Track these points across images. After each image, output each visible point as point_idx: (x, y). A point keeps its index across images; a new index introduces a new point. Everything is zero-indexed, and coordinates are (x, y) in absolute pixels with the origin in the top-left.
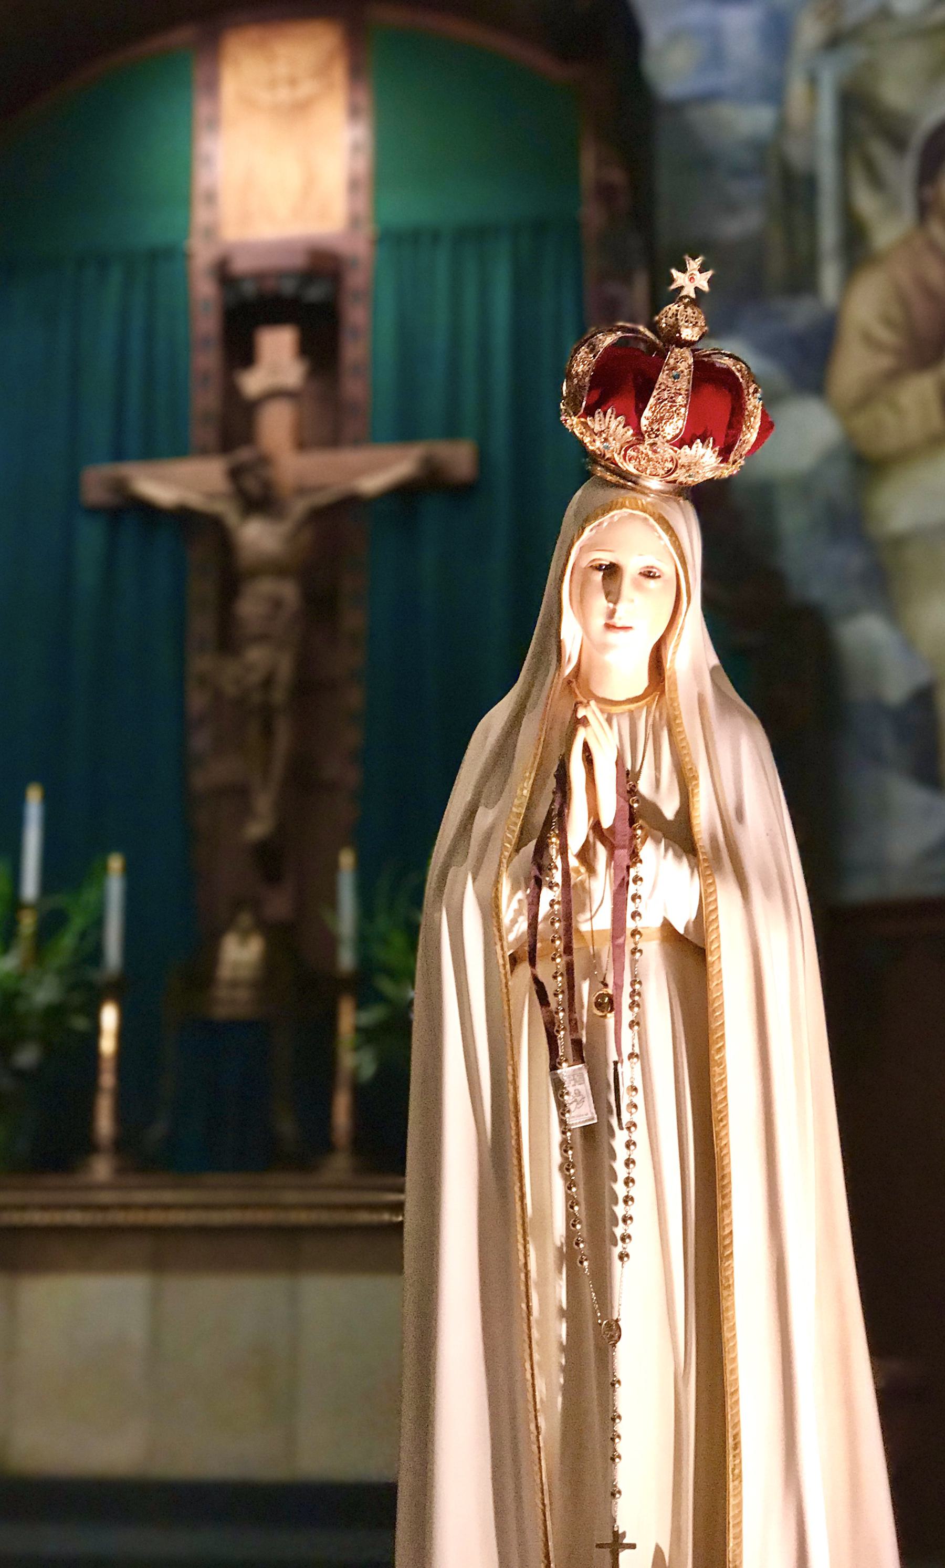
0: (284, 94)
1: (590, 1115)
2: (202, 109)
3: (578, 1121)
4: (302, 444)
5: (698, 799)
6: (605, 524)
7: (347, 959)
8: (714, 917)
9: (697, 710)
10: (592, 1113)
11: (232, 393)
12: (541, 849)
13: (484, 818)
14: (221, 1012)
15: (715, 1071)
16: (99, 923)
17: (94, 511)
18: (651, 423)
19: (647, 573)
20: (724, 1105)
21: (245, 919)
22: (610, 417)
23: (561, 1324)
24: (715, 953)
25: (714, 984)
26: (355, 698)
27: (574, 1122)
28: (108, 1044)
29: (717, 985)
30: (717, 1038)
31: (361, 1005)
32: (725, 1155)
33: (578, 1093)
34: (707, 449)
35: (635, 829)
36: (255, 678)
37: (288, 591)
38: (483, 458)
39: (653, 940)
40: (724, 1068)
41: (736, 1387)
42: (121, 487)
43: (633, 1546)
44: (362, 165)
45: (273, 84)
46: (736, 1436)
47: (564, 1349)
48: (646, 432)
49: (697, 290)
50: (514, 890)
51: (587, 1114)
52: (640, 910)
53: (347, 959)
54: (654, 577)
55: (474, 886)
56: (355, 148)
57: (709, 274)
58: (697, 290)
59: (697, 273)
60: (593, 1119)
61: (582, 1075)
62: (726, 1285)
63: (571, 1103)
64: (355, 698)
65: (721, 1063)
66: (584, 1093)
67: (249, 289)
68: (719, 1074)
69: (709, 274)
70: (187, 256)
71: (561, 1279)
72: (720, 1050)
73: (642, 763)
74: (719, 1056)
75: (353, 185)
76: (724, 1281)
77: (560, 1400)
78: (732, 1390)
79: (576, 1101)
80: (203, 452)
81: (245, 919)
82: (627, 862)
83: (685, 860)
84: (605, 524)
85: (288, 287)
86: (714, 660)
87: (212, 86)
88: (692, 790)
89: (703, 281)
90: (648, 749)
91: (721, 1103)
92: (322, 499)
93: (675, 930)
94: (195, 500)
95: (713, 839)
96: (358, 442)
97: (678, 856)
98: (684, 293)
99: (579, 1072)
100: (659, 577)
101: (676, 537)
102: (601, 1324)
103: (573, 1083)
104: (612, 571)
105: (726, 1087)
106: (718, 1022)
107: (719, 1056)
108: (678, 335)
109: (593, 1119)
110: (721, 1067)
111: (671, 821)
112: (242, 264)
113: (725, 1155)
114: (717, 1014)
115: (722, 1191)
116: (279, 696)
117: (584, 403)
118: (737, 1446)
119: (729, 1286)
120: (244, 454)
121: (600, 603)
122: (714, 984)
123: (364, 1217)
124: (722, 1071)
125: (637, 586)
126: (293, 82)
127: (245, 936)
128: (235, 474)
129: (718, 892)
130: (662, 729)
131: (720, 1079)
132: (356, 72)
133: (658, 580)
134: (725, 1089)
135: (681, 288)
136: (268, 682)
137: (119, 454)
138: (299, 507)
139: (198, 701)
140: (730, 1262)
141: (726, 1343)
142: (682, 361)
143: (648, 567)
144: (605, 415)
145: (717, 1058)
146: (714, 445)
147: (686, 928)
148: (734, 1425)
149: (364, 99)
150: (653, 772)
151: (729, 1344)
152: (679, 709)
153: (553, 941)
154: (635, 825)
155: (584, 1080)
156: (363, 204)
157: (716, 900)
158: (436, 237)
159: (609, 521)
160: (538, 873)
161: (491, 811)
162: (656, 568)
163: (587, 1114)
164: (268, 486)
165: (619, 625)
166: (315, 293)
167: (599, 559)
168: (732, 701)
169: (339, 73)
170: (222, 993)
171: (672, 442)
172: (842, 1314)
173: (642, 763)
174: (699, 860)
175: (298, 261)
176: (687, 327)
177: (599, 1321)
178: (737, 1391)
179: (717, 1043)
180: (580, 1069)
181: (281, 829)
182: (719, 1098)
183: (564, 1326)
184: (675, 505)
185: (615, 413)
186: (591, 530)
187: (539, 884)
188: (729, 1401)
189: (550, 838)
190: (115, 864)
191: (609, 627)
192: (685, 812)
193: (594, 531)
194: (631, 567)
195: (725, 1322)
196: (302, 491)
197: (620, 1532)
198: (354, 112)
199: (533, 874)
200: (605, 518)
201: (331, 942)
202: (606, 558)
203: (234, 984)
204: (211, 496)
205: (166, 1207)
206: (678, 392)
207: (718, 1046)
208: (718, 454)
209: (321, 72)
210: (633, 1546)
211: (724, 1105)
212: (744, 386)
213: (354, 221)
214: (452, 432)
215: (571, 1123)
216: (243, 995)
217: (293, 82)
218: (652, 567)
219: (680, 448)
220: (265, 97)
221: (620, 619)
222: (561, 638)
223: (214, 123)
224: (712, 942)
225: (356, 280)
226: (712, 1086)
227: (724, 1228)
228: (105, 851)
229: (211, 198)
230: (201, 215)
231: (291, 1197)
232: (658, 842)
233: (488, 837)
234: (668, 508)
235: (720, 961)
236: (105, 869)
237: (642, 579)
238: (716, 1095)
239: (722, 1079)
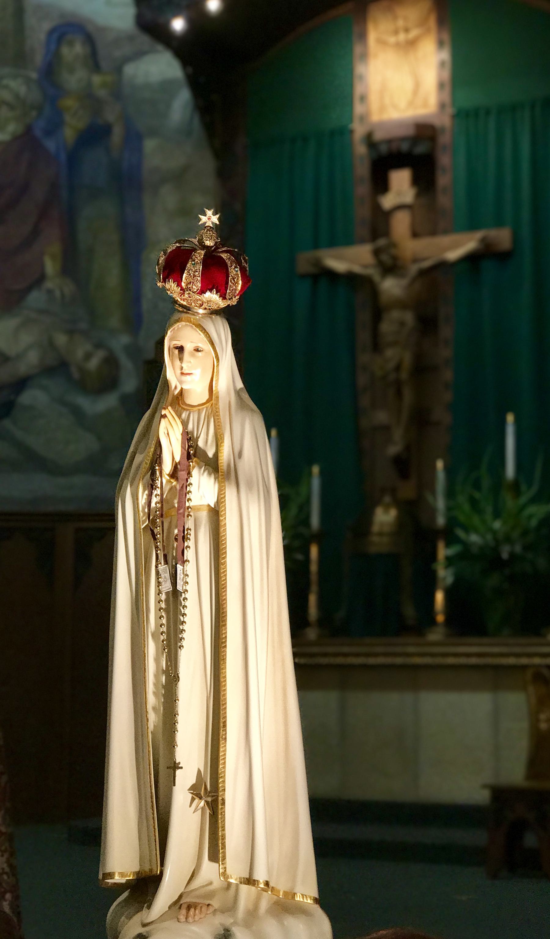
0: (402, 37)
1: (169, 587)
2: (358, 49)
3: (165, 589)
4: (415, 235)
5: (223, 448)
6: (176, 329)
7: (441, 521)
8: (223, 500)
9: (228, 409)
10: (170, 586)
11: (377, 208)
12: (153, 473)
13: (138, 458)
14: (373, 550)
15: (221, 567)
16: (308, 501)
17: (304, 276)
18: (187, 285)
19: (197, 349)
20: (224, 582)
21: (387, 499)
22: (171, 283)
23: (163, 676)
24: (223, 516)
25: (222, 529)
26: (448, 375)
27: (164, 590)
28: (314, 568)
29: (224, 530)
30: (223, 553)
31: (448, 545)
32: (224, 603)
33: (165, 578)
34: (213, 294)
35: (189, 463)
36: (391, 365)
37: (409, 317)
38: (516, 237)
39: (205, 511)
40: (226, 566)
41: (225, 702)
42: (318, 263)
43: (181, 768)
44: (446, 74)
45: (396, 32)
46: (225, 722)
47: (164, 687)
48: (185, 288)
49: (213, 223)
50: (144, 491)
51: (168, 586)
52: (191, 498)
53: (441, 521)
54: (200, 351)
55: (130, 488)
56: (442, 64)
57: (218, 216)
58: (213, 223)
59: (212, 216)
60: (170, 589)
61: (167, 569)
62: (222, 659)
63: (163, 582)
64: (448, 375)
65: (225, 563)
66: (167, 577)
67: (384, 149)
68: (223, 568)
69: (218, 216)
70: (351, 132)
71: (164, 658)
72: (224, 558)
73: (201, 432)
74: (223, 561)
75: (441, 86)
76: (221, 657)
77: (162, 708)
78: (223, 703)
79: (164, 581)
80: (362, 241)
81: (387, 499)
82: (186, 477)
83: (213, 476)
84: (176, 329)
85: (405, 147)
86: (240, 385)
87: (363, 36)
88: (220, 444)
89: (215, 219)
90: (204, 426)
91: (223, 581)
92: (426, 264)
93: (212, 507)
94: (357, 269)
95: (229, 466)
96: (446, 232)
97: (210, 474)
98: (207, 225)
99: (165, 568)
100: (202, 351)
101: (207, 333)
102: (171, 675)
103: (163, 573)
104: (181, 349)
105: (226, 574)
106: (223, 546)
107: (223, 561)
108: (203, 244)
109: (170, 589)
110: (224, 565)
111: (211, 458)
112: (378, 136)
113: (224, 603)
114: (223, 542)
115: (222, 619)
116: (404, 375)
117: (161, 276)
118: (225, 726)
119: (224, 659)
120: (382, 242)
121: (178, 363)
122: (222, 529)
123: (451, 661)
124: (224, 567)
125: (192, 355)
126: (407, 30)
127: (387, 508)
128: (377, 253)
129: (227, 489)
130: (211, 418)
131: (223, 570)
132: (441, 22)
133: (201, 352)
134: (226, 575)
135: (205, 223)
136: (398, 368)
137: (316, 246)
138: (414, 269)
139: (362, 380)
140: (225, 649)
141: (221, 683)
142: (199, 255)
143: (196, 347)
144: (169, 281)
145: (222, 561)
146: (217, 293)
147: (215, 505)
148: (223, 717)
149: (446, 37)
150: (206, 437)
151: (222, 684)
152: (219, 409)
153: (156, 512)
154: (189, 461)
155: (167, 572)
156: (447, 96)
157: (225, 493)
158: (488, 112)
159: (177, 327)
160: (152, 483)
161: (141, 455)
162: (201, 348)
163: (168, 586)
164: (395, 258)
165: (185, 373)
166: (421, 149)
167: (176, 344)
168: (248, 405)
169: (432, 22)
170: (375, 539)
171: (197, 292)
172: (284, 673)
173: (201, 432)
174: (219, 475)
175: (411, 132)
176: (207, 240)
177: (171, 674)
178: (226, 704)
179: (223, 555)
180: (166, 567)
181: (408, 448)
182: (223, 579)
183: (164, 677)
184: (209, 319)
185: (172, 281)
186: (171, 332)
187: (152, 488)
188: (221, 707)
189: (155, 467)
190: (316, 470)
191: (182, 374)
192: (216, 455)
193: (172, 332)
194: (189, 347)
195: (221, 674)
196: (415, 260)
197: (177, 762)
198: (441, 44)
199: (150, 483)
200: (175, 326)
201: (433, 511)
202: (179, 344)
203: (380, 534)
204: (365, 266)
205: (345, 655)
206: (196, 271)
207: (223, 556)
208: (220, 296)
209: (422, 23)
210: (181, 768)
211: (224, 582)
212: (229, 265)
213: (442, 106)
214: (499, 223)
215: (162, 590)
216: (385, 540)
217: (407, 30)
218: (198, 347)
219: (201, 295)
220: (392, 40)
221: (185, 370)
222: (168, 379)
223: (364, 56)
224: (222, 510)
225: (444, 139)
226: (220, 574)
227: (222, 634)
228: (310, 464)
229: (363, 99)
230: (358, 109)
231: (411, 649)
232: (200, 468)
233: (139, 467)
234: (204, 321)
235: (225, 519)
236: (310, 474)
237: (194, 352)
238: (221, 577)
239: (224, 571)
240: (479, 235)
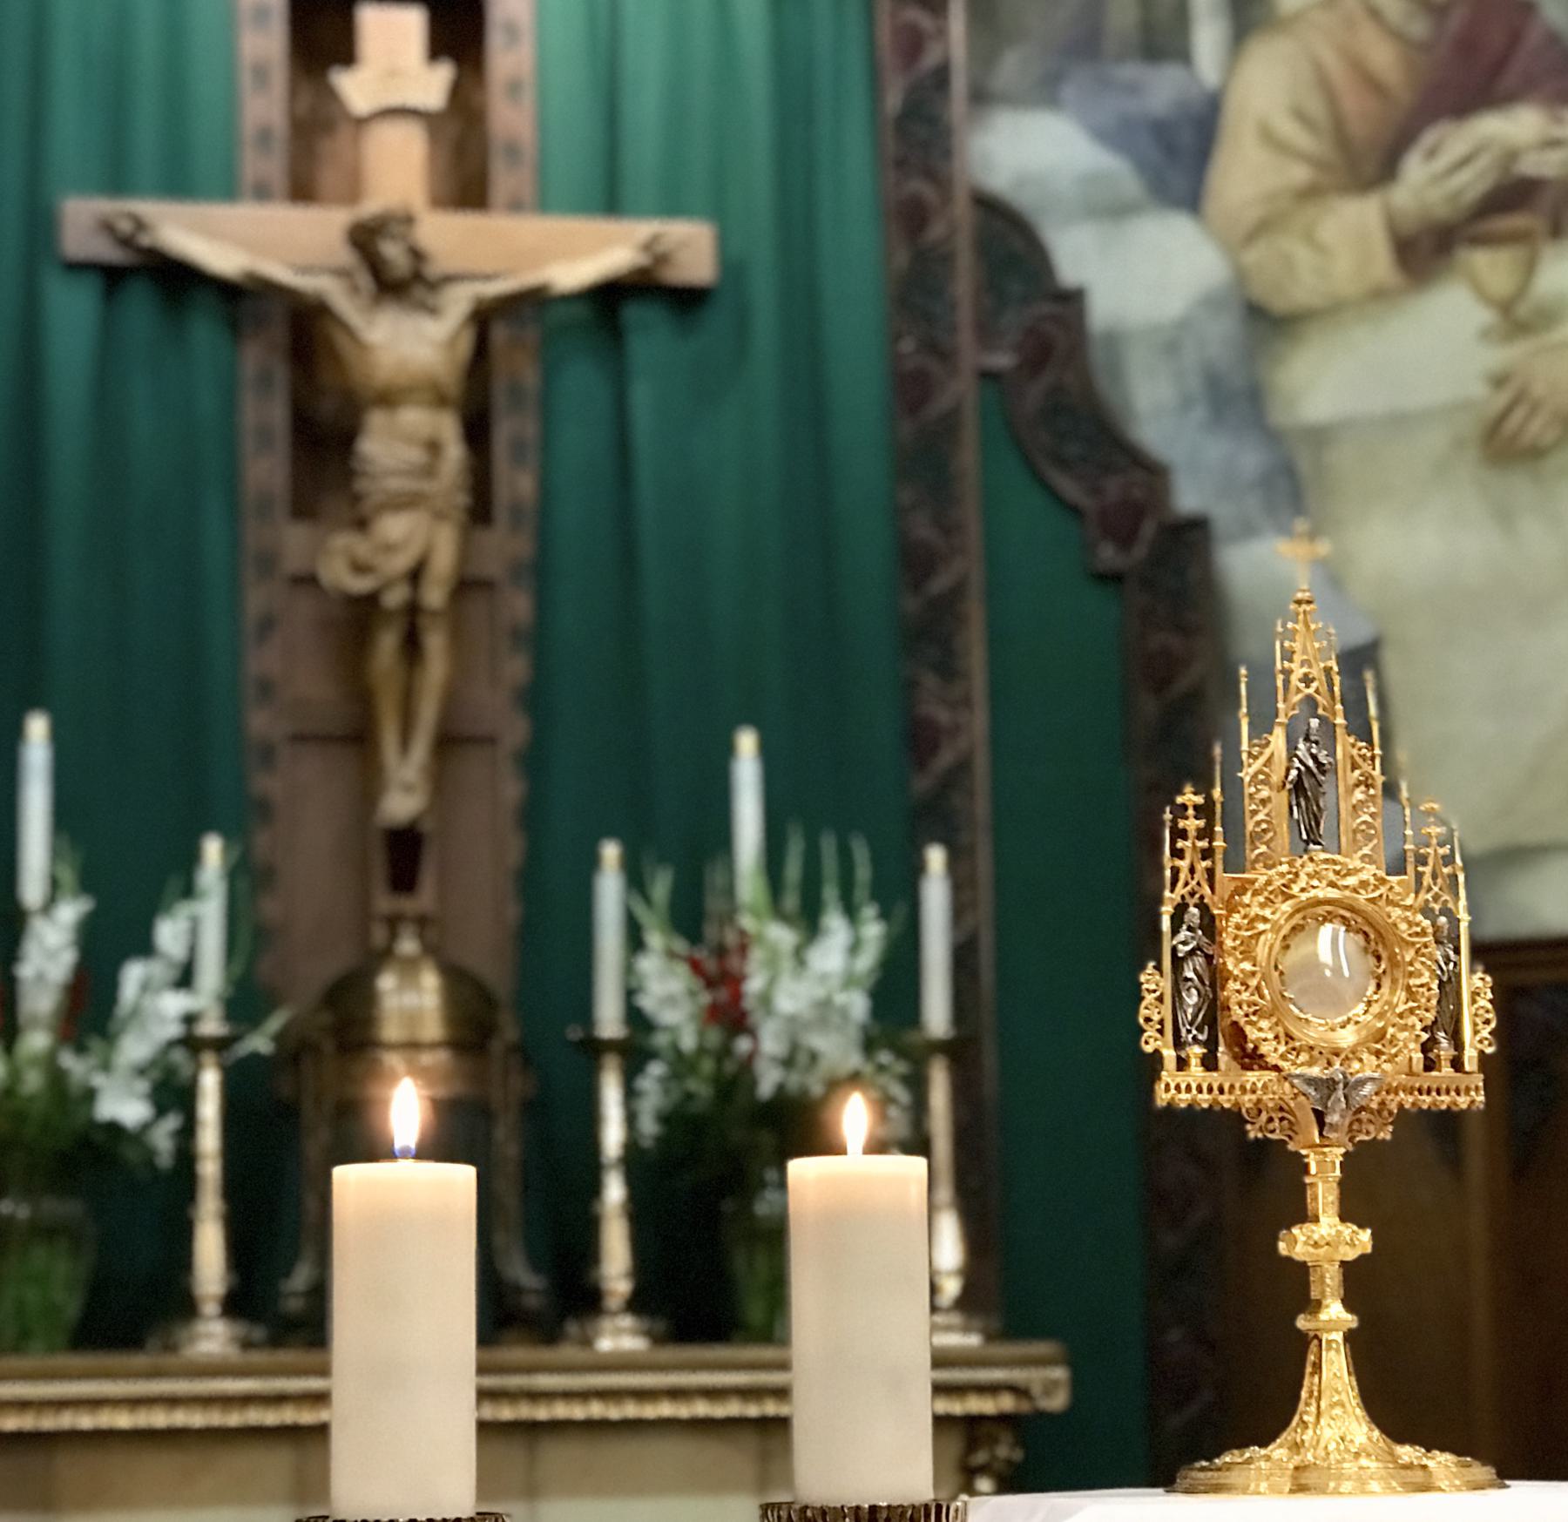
116: (434, 595)
136: (415, 575)
240: (639, 230)
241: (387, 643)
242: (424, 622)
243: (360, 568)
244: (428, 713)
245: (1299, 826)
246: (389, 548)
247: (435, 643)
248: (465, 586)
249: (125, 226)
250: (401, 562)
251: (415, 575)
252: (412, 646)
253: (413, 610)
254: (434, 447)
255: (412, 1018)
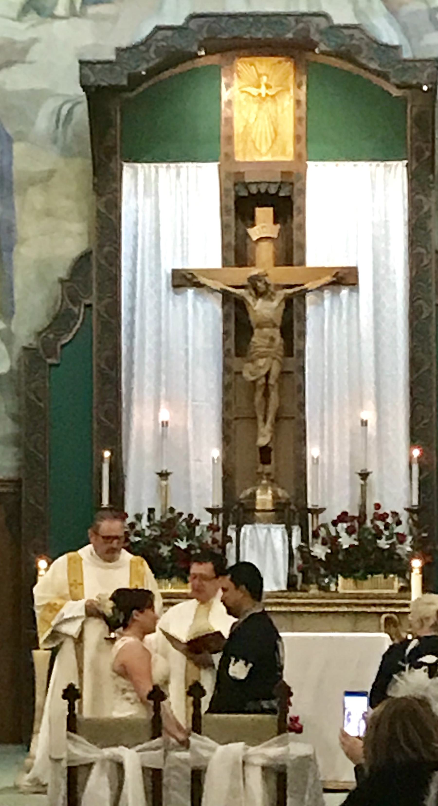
85: (273, 190)
136: (267, 376)
241: (259, 395)
242: (270, 388)
243: (252, 374)
244: (271, 417)
245: (66, 344)
246: (260, 367)
247: (274, 395)
248: (284, 373)
249: (189, 276)
250: (263, 372)
251: (267, 376)
252: (266, 395)
253: (267, 385)
254: (272, 339)
255: (264, 504)
